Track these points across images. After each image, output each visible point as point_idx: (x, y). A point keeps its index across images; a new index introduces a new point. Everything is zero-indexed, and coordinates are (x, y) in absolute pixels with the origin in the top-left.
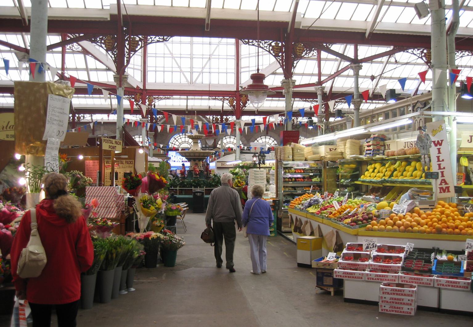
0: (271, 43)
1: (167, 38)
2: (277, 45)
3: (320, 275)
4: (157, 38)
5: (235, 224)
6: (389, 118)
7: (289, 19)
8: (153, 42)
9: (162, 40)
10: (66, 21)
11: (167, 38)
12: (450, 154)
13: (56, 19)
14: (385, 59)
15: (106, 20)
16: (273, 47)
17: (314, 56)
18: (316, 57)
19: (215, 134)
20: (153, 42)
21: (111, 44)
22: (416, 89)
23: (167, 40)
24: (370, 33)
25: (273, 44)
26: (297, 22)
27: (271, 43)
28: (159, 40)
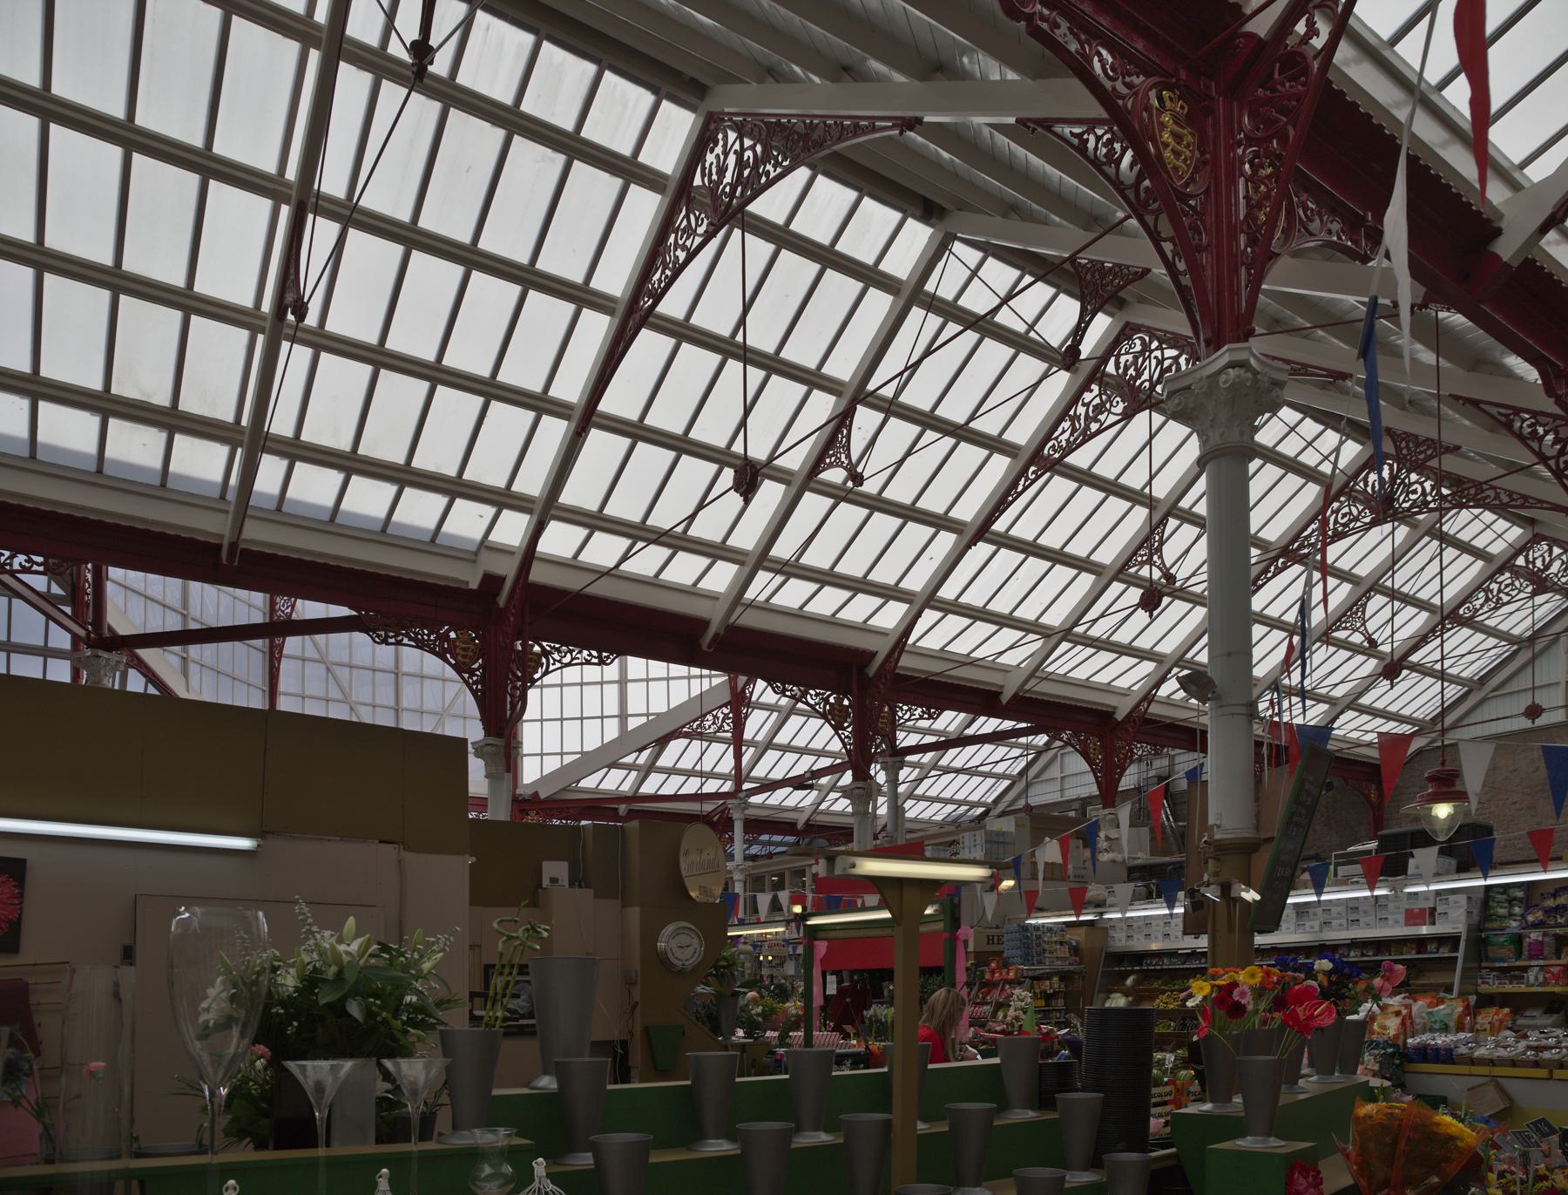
0: (829, 696)
1: (608, 657)
2: (839, 701)
3: (1324, 638)
4: (585, 653)
5: (821, 960)
6: (431, 1139)
7: (882, 648)
8: (574, 662)
9: (596, 661)
10: (287, 559)
11: (608, 657)
12: (1041, 910)
13: (80, 515)
14: (928, 757)
15: (464, 587)
16: (831, 704)
17: (725, 731)
18: (730, 735)
19: (414, 951)
20: (574, 662)
21: (471, 654)
22: (1001, 819)
23: (609, 661)
24: (1015, 695)
25: (832, 700)
26: (256, 493)
27: (829, 696)
28: (27, 565)
